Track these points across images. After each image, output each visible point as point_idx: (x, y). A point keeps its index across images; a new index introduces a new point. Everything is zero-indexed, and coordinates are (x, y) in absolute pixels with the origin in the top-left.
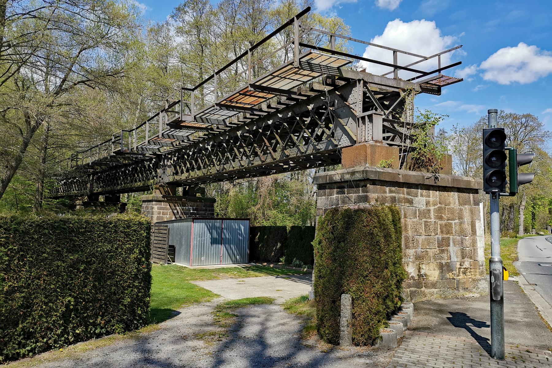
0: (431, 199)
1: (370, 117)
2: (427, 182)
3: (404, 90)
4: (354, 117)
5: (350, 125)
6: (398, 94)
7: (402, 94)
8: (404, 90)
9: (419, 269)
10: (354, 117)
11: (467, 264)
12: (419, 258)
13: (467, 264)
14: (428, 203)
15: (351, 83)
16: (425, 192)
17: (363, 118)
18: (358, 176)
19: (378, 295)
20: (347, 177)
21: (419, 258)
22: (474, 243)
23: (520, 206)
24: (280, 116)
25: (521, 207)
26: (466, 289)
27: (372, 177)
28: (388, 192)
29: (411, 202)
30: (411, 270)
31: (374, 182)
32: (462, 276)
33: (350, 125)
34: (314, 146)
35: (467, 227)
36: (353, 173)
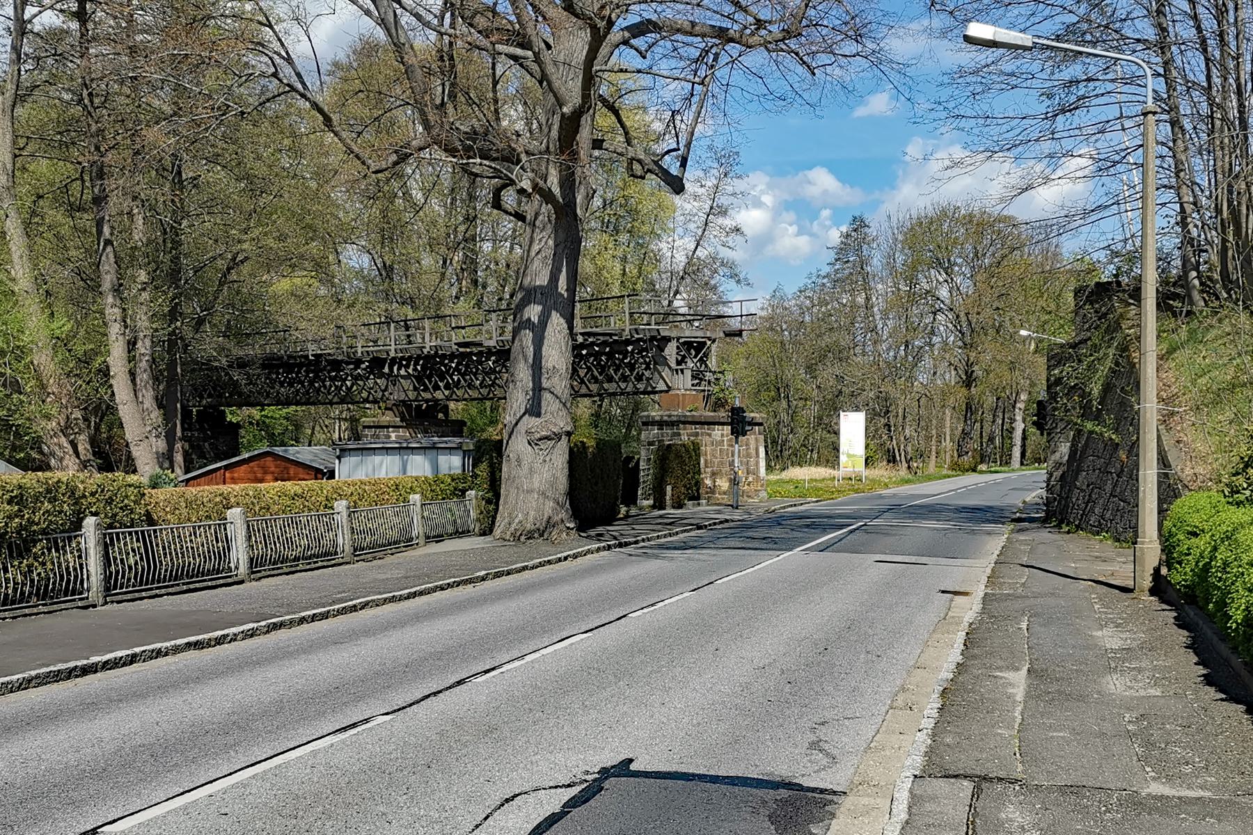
0: (725, 432)
1: (682, 371)
2: (722, 420)
3: (709, 339)
4: (670, 368)
5: (666, 373)
6: (705, 343)
7: (709, 343)
8: (709, 339)
9: (715, 482)
10: (670, 368)
11: (750, 479)
12: (714, 474)
13: (750, 479)
14: (722, 435)
15: (667, 340)
16: (720, 427)
17: (677, 370)
18: (675, 419)
19: (685, 486)
20: (665, 418)
21: (714, 474)
22: (757, 463)
23: (1015, 402)
24: (597, 349)
25: (1018, 405)
26: (748, 496)
27: (683, 419)
28: (691, 429)
29: (710, 435)
30: (708, 482)
31: (684, 423)
32: (746, 487)
33: (666, 373)
34: (635, 385)
35: (753, 452)
36: (670, 416)
